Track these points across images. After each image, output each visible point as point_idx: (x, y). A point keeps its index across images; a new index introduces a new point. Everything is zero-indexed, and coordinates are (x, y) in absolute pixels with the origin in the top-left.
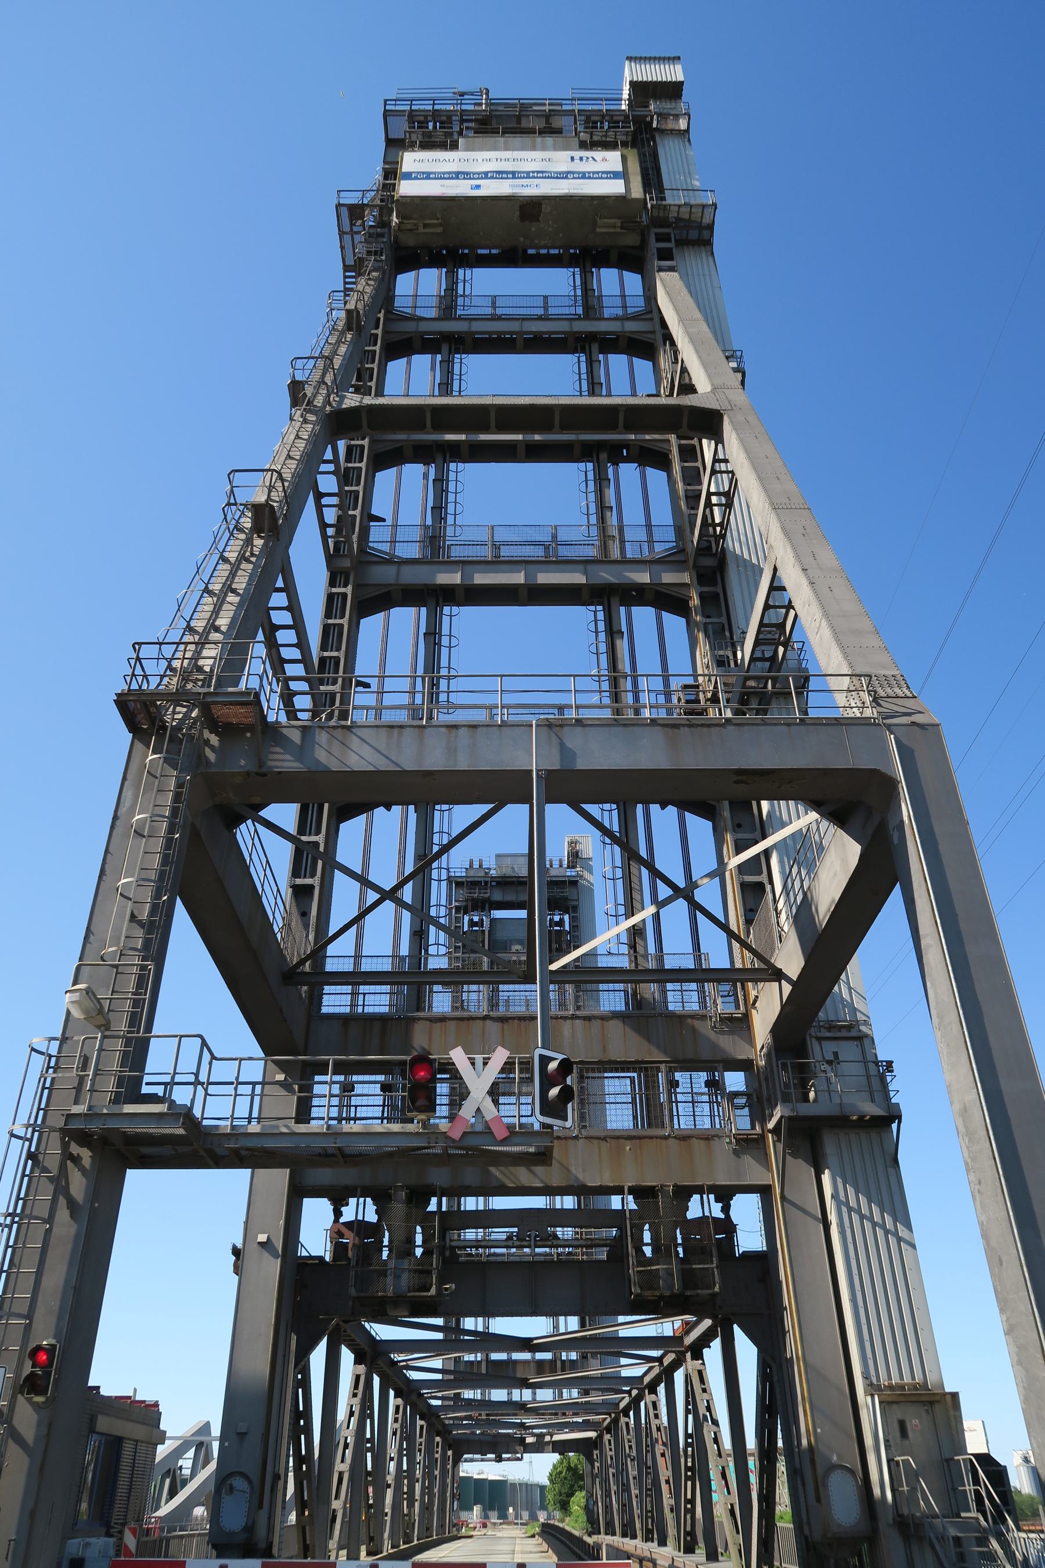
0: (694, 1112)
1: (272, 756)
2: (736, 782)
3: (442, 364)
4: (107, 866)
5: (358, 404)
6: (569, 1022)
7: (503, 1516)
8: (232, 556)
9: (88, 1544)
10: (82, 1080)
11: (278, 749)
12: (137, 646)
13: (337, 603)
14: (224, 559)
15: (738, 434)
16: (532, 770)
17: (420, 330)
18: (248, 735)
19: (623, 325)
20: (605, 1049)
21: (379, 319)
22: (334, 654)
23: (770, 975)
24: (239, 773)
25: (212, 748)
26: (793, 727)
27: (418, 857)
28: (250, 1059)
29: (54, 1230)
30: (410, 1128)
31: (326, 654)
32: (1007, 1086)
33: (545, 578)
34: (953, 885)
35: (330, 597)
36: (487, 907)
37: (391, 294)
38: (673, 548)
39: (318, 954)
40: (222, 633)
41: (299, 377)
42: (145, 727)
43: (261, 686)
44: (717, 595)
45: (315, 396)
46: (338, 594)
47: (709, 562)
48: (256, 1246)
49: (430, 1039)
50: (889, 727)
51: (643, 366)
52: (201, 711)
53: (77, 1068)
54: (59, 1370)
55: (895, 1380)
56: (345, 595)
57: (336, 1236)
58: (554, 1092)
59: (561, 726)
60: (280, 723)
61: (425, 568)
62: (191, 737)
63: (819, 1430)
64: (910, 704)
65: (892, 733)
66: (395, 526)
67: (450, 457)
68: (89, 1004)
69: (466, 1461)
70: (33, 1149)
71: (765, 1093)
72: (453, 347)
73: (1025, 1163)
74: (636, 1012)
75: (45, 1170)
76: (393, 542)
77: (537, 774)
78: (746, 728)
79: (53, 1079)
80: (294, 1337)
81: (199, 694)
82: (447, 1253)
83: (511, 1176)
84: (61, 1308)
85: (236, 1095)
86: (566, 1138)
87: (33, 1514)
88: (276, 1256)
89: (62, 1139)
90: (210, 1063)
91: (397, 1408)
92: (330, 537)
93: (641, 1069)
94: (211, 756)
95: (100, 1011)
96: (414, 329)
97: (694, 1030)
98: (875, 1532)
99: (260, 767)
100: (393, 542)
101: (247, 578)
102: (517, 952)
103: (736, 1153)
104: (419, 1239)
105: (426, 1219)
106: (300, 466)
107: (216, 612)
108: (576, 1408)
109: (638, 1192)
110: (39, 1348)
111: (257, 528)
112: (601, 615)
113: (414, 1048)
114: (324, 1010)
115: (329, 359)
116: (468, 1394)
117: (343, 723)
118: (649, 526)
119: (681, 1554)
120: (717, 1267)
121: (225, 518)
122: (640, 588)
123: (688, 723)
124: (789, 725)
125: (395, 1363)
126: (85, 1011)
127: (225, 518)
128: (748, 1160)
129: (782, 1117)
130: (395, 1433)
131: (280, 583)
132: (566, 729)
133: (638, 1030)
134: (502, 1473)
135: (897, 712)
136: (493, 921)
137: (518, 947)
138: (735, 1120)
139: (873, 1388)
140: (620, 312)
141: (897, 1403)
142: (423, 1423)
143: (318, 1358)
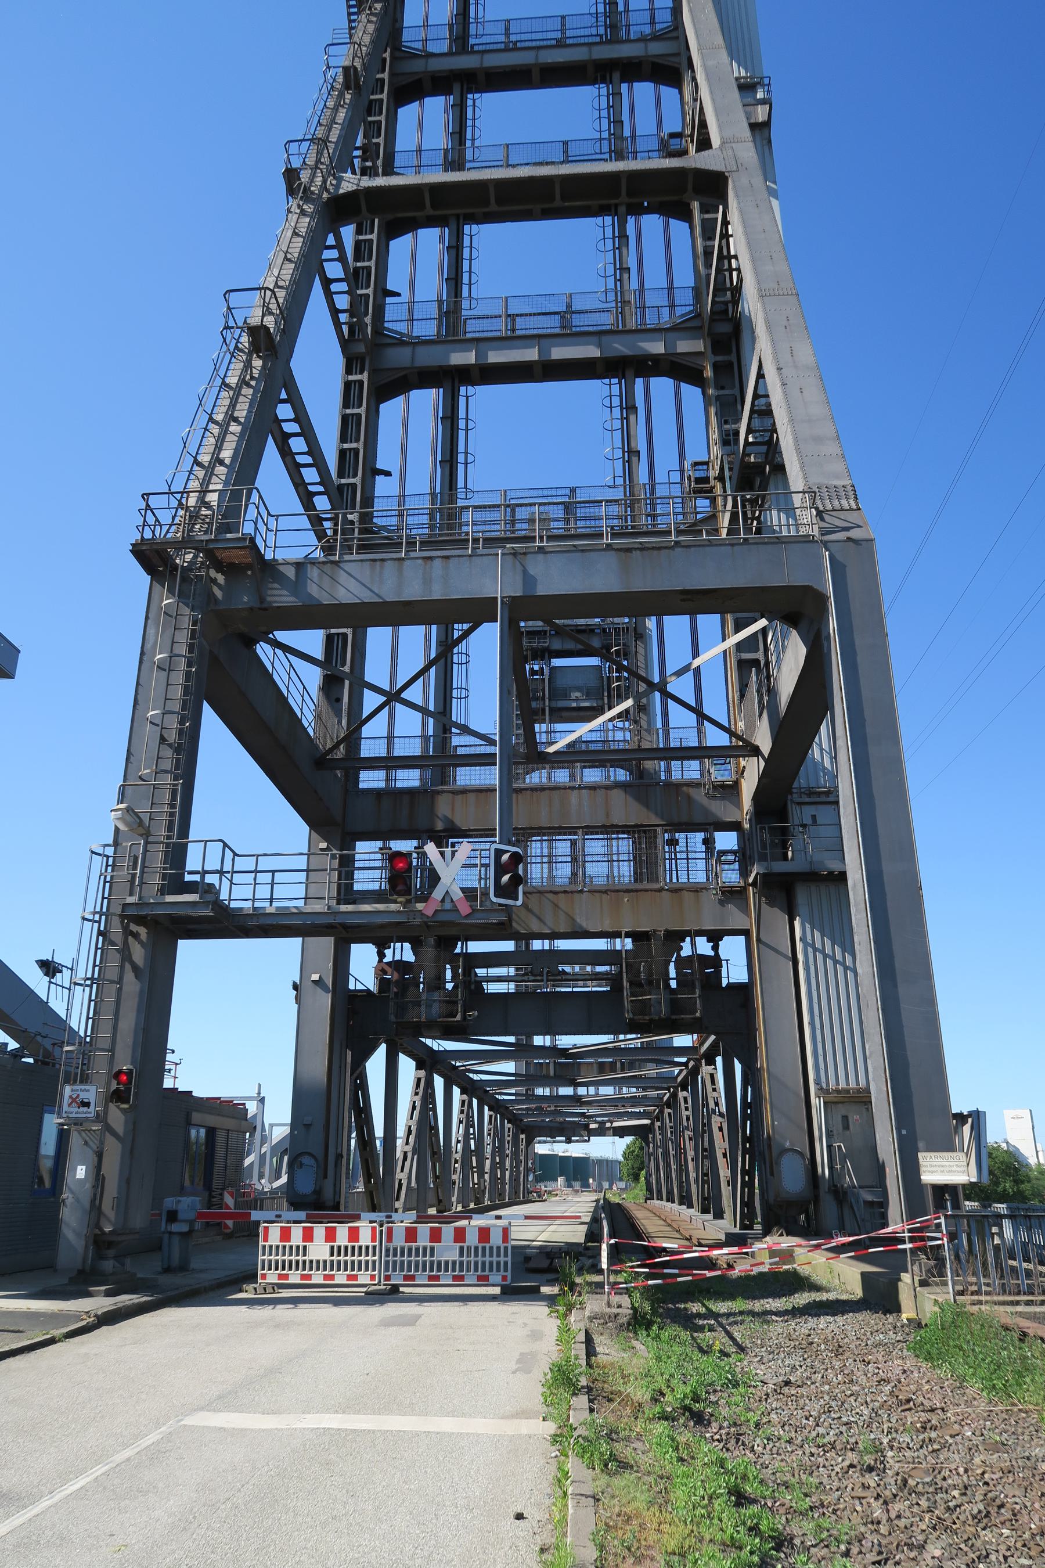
0: (688, 867)
1: (269, 592)
2: (683, 600)
3: (454, 108)
4: (139, 697)
5: (355, 187)
6: (576, 791)
7: (585, 1185)
8: (233, 380)
9: (179, 1201)
10: (134, 876)
11: (276, 586)
12: (145, 496)
13: (354, 390)
14: (225, 385)
15: (739, 203)
16: (497, 598)
17: (429, 69)
18: (249, 573)
19: (646, 48)
20: (608, 815)
21: (385, 59)
22: (354, 445)
23: (749, 751)
24: (243, 609)
25: (219, 586)
26: (736, 548)
27: (439, 643)
28: (265, 855)
29: (124, 987)
30: (393, 907)
31: (346, 446)
32: (888, 868)
33: (559, 353)
34: (866, 693)
35: (347, 385)
36: (547, 656)
37: (398, 25)
38: (691, 312)
39: (353, 738)
40: (226, 466)
41: (296, 163)
42: (161, 569)
43: (256, 528)
44: (731, 364)
45: (312, 180)
46: (355, 381)
47: (724, 328)
48: (310, 983)
49: (453, 809)
50: (826, 544)
51: (668, 93)
52: (206, 556)
53: (128, 865)
54: (137, 1086)
55: (842, 1085)
56: (361, 383)
57: (381, 973)
58: (506, 878)
59: (525, 554)
60: (277, 560)
61: (439, 349)
62: (199, 578)
63: (776, 1123)
64: (853, 517)
65: (827, 550)
66: (412, 302)
67: (464, 220)
68: (128, 818)
69: (540, 1142)
70: (102, 928)
71: (748, 853)
72: (465, 87)
73: (893, 929)
74: (637, 781)
75: (113, 944)
76: (411, 320)
77: (502, 601)
78: (693, 549)
79: (112, 877)
80: (349, 1053)
81: (202, 541)
82: (473, 987)
83: (523, 924)
84: (134, 1043)
85: (256, 884)
86: (571, 892)
87: (128, 1182)
88: (327, 991)
89: (122, 922)
90: (233, 860)
91: (491, 1117)
92: (344, 323)
93: (639, 832)
94: (218, 593)
95: (141, 823)
96: (423, 69)
97: (689, 798)
98: (816, 1199)
99: (262, 602)
100: (411, 320)
101: (248, 404)
102: (577, 700)
103: (722, 903)
104: (449, 975)
105: (454, 959)
106: (296, 273)
107: (219, 447)
108: (634, 1101)
109: (635, 936)
110: (120, 1072)
111: (255, 348)
112: (615, 390)
113: (438, 817)
114: (362, 785)
115: (325, 141)
116: (539, 1091)
117: (331, 558)
118: (671, 289)
119: (699, 1214)
120: (699, 997)
121: (225, 340)
122: (656, 358)
123: (640, 546)
124: (732, 545)
125: (456, 1068)
126: (126, 824)
127: (225, 340)
128: (731, 908)
129: (757, 874)
130: (489, 1134)
131: (284, 395)
132: (529, 556)
133: (638, 798)
134: (584, 1152)
135: (837, 527)
136: (553, 669)
137: (578, 694)
138: (721, 874)
139: (822, 1091)
140: (647, 30)
141: (843, 1103)
142: (510, 1125)
143: (376, 1066)
